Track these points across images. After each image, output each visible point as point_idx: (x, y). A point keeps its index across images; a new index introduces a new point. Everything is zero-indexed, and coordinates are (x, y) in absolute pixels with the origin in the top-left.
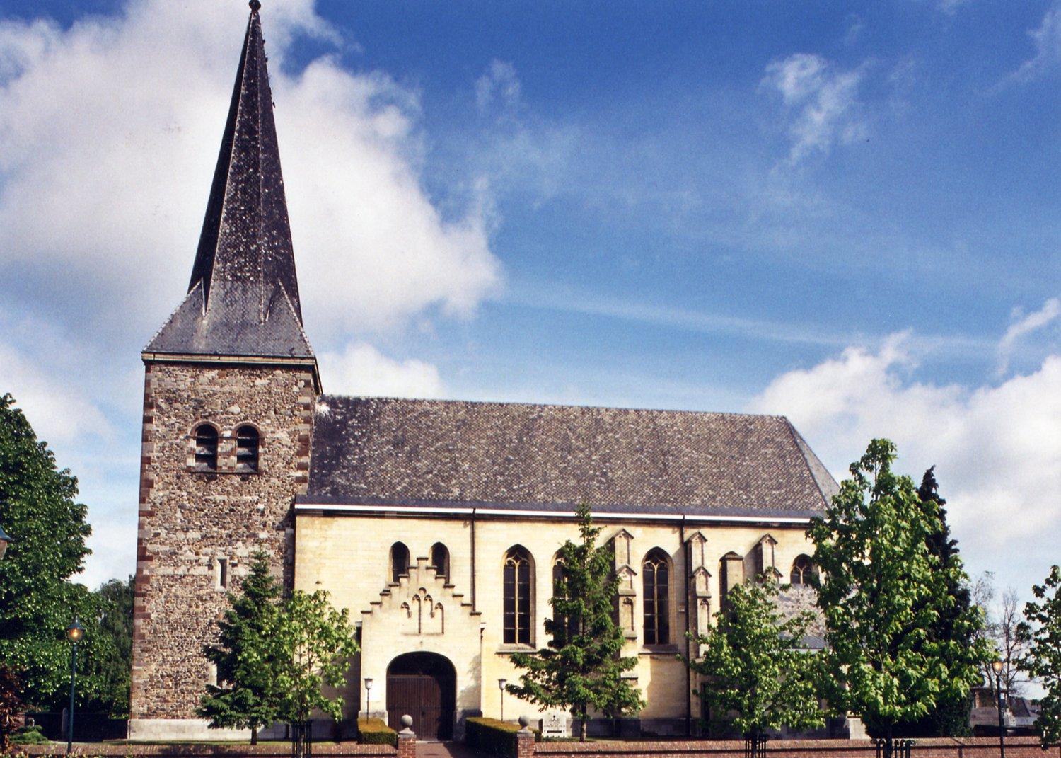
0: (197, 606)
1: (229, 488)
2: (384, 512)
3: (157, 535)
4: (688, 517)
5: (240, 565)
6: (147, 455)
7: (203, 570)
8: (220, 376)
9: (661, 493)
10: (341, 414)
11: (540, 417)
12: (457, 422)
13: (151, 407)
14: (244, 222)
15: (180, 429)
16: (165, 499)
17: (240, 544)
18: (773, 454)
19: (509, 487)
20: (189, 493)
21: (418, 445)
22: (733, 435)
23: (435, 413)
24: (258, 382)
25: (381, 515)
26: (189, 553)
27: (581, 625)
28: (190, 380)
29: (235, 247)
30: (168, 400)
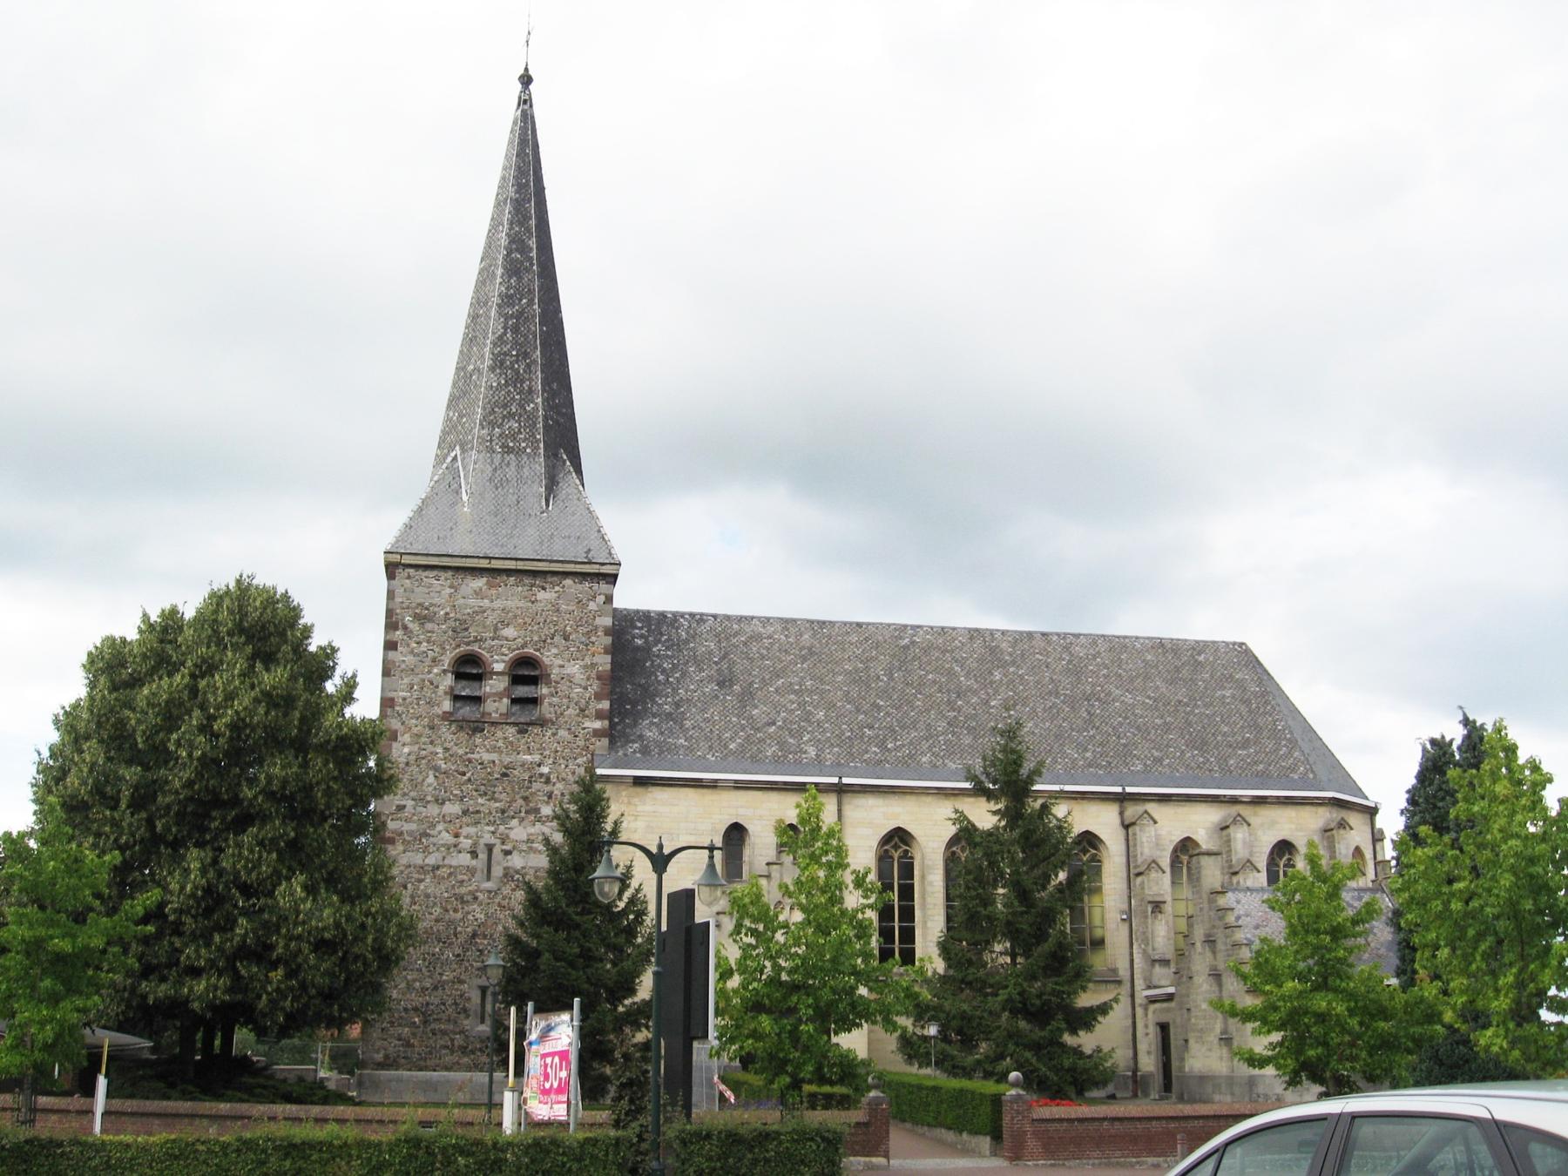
0: (456, 911)
1: (500, 744)
2: (716, 781)
3: (401, 808)
4: (1129, 790)
5: (515, 853)
6: (392, 694)
7: (465, 859)
8: (490, 586)
9: (1088, 754)
10: (642, 636)
11: (913, 642)
12: (801, 649)
13: (396, 628)
14: (517, 372)
15: (434, 660)
16: (412, 757)
17: (515, 822)
18: (1233, 696)
19: (882, 745)
20: (446, 749)
21: (751, 684)
22: (1177, 670)
23: (770, 637)
24: (541, 595)
25: (713, 785)
26: (444, 834)
27: (719, 867)
28: (449, 591)
29: (505, 406)
30: (416, 617)
